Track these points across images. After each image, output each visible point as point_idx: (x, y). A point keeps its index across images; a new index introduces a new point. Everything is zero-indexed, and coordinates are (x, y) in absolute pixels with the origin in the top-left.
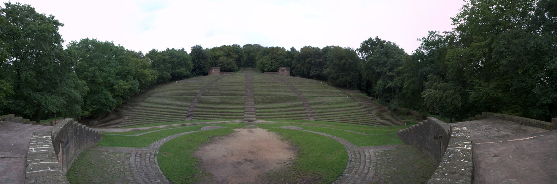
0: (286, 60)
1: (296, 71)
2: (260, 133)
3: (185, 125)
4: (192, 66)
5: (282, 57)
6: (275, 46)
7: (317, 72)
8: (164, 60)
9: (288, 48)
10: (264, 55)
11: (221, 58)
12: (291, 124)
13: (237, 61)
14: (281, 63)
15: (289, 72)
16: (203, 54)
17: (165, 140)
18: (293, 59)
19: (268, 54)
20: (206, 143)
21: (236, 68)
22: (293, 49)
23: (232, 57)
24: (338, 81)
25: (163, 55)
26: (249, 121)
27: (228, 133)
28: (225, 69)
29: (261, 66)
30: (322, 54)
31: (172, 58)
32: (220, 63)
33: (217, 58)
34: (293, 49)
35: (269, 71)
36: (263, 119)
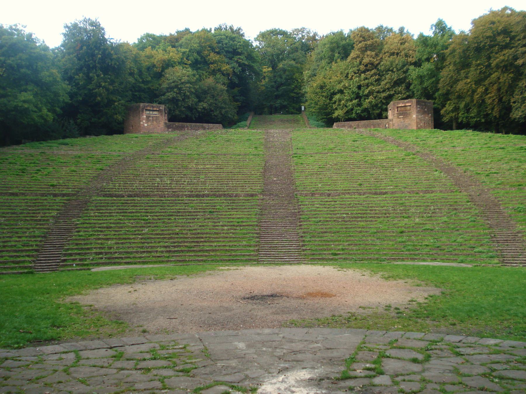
1: (456, 109)
9: (420, 27)
10: (331, 59)
13: (231, 85)
14: (397, 83)
23: (213, 73)
28: (188, 113)
29: (322, 101)
32: (170, 89)
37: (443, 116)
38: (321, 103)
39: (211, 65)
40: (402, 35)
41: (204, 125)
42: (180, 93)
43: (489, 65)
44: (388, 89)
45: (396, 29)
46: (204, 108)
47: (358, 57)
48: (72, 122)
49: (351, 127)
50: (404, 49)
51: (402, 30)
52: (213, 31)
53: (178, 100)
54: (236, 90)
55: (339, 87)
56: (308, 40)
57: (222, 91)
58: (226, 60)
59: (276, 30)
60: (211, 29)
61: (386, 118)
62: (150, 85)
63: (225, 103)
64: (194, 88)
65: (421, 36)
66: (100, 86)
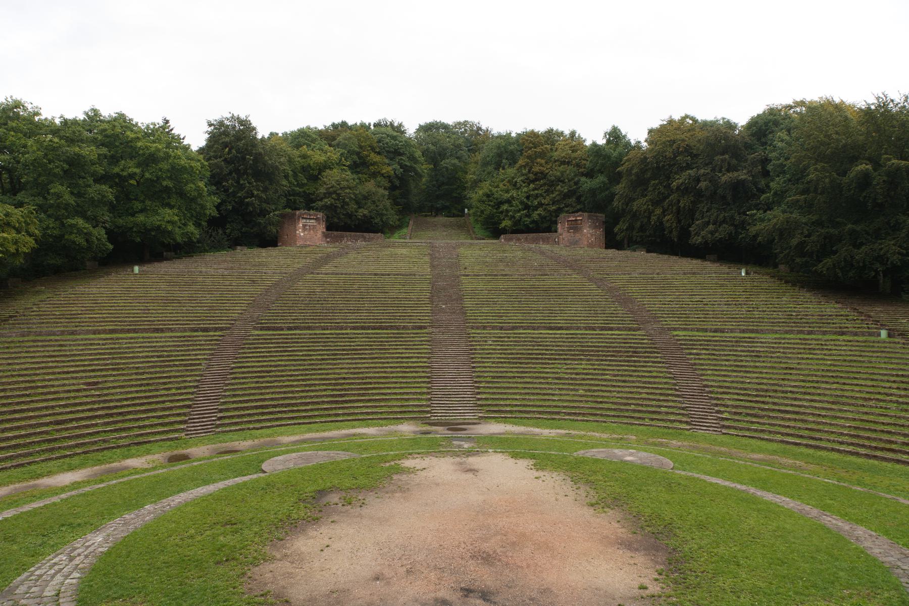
0: (587, 184)
1: (631, 228)
2: (504, 474)
3: (185, 458)
4: (210, 203)
5: (569, 170)
6: (541, 128)
7: (724, 231)
8: (75, 165)
9: (593, 135)
10: (498, 166)
11: (333, 176)
12: (622, 443)
13: (393, 188)
14: (566, 196)
15: (600, 232)
16: (258, 157)
17: (98, 541)
18: (616, 178)
19: (513, 161)
20: (292, 525)
21: (392, 217)
22: (615, 136)
23: (374, 175)
24: (828, 261)
25: (71, 141)
26: (453, 427)
27: (372, 478)
29: (488, 210)
30: (748, 146)
31: (114, 160)
32: (328, 194)
33: (314, 173)
34: (615, 136)
35: (520, 229)
36: (505, 420)
37: (616, 234)
38: (487, 212)
39: (371, 167)
40: (572, 140)
41: (365, 234)
42: (338, 199)
43: (668, 186)
44: (558, 201)
45: (567, 132)
46: (364, 215)
47: (527, 164)
48: (220, 231)
49: (519, 240)
50: (576, 158)
51: (573, 134)
52: (372, 127)
53: (336, 207)
54: (397, 192)
55: (506, 196)
56: (471, 136)
57: (383, 196)
58: (387, 161)
59: (437, 123)
60: (370, 124)
61: (556, 232)
62: (306, 188)
63: (387, 210)
64: (354, 194)
65: (594, 145)
66: (253, 195)
